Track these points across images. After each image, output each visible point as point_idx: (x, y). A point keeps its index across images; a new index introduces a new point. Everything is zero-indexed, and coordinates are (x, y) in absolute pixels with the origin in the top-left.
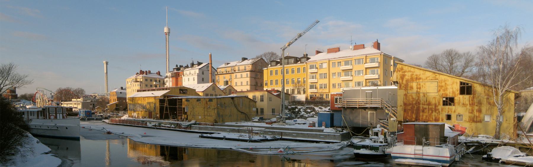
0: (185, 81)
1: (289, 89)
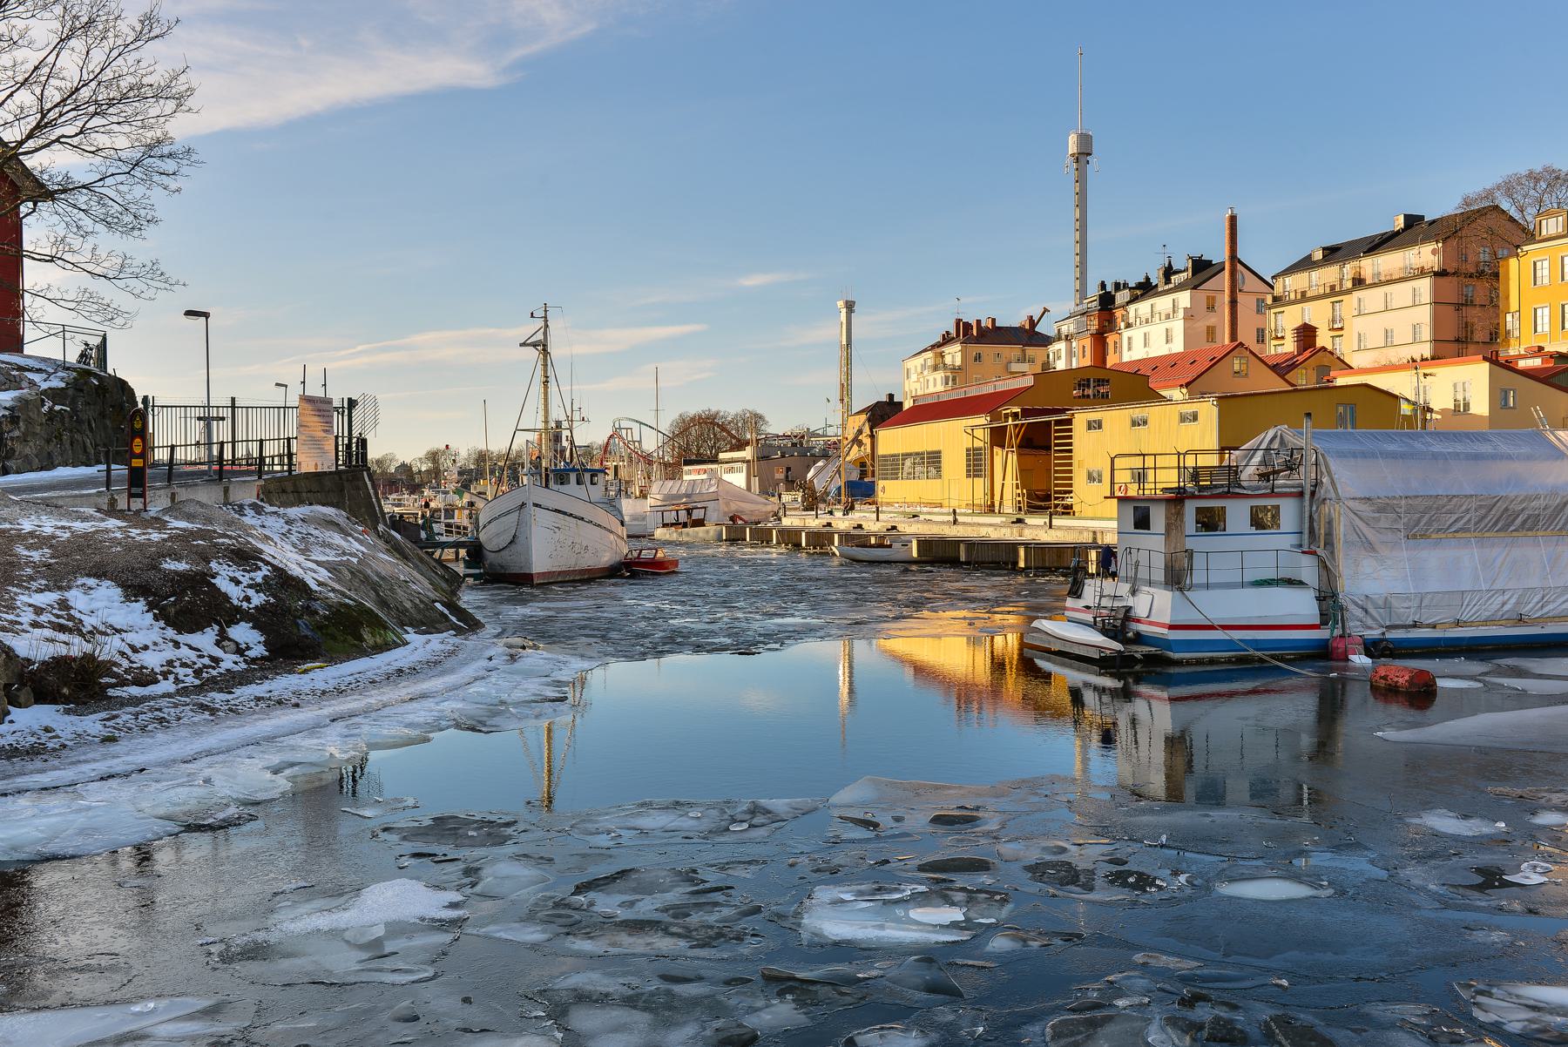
0: (1227, 224)
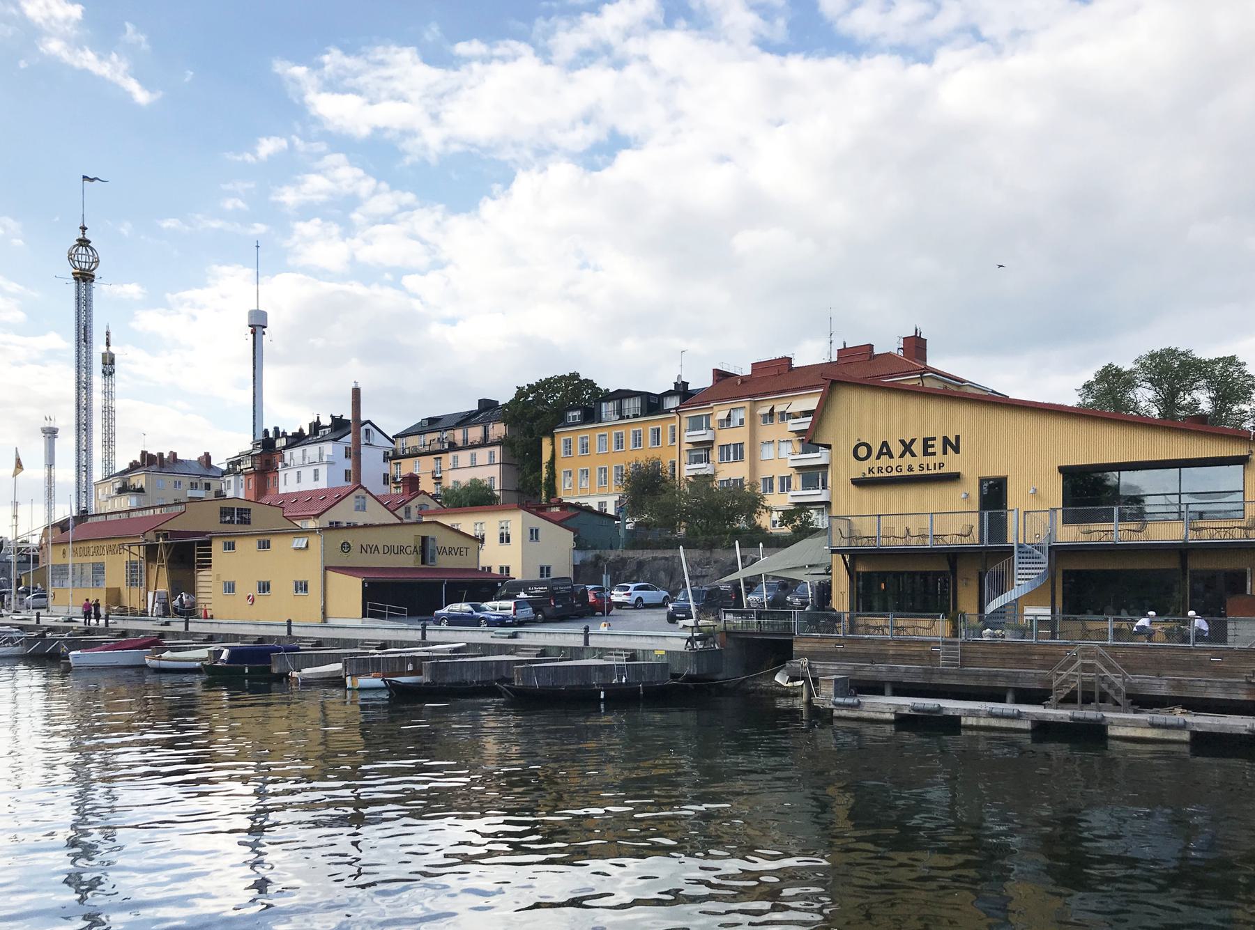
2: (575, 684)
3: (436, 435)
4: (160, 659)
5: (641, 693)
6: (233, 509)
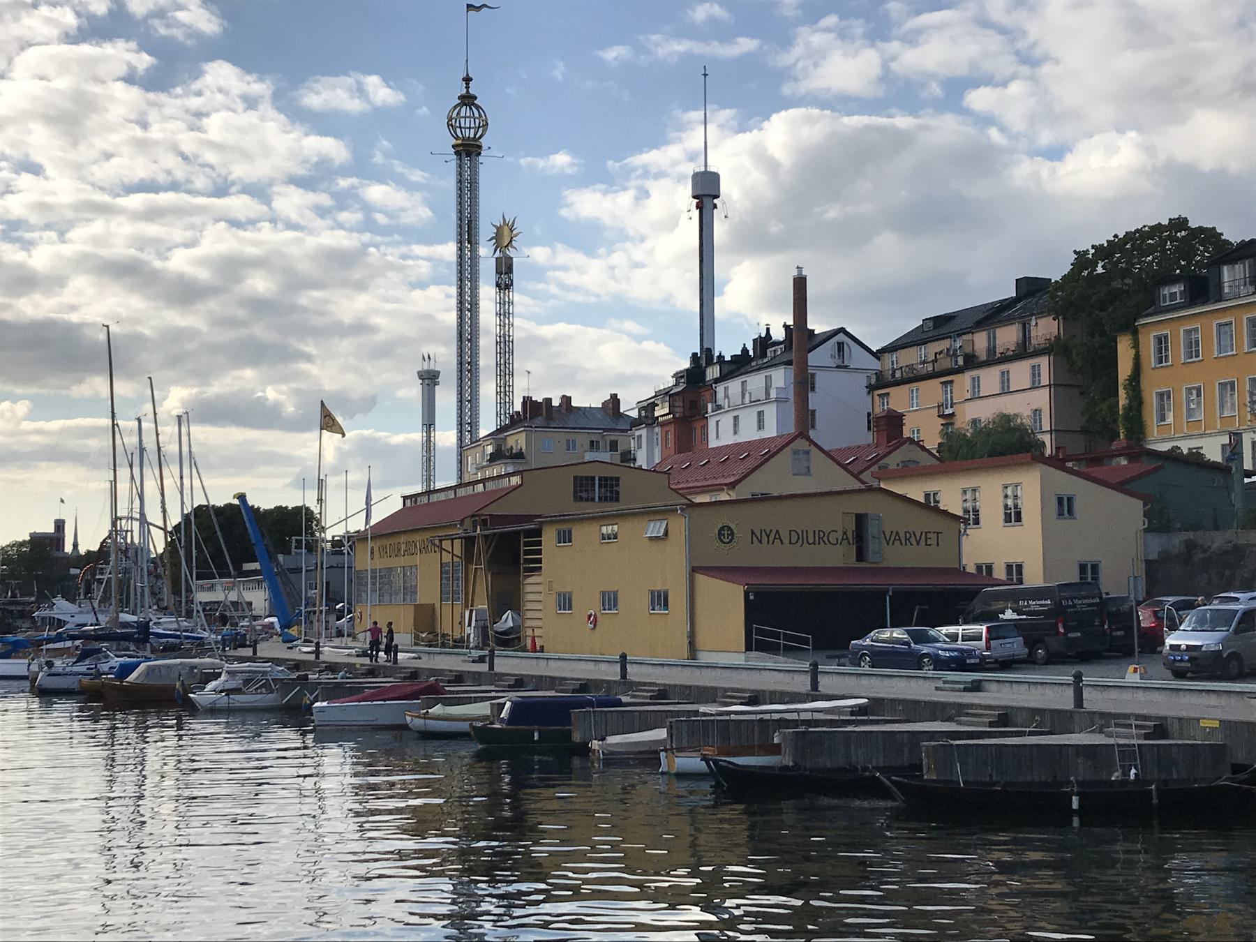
1: (575, 478)
2: (1036, 779)
3: (944, 345)
4: (426, 716)
5: (1155, 801)
6: (593, 478)
